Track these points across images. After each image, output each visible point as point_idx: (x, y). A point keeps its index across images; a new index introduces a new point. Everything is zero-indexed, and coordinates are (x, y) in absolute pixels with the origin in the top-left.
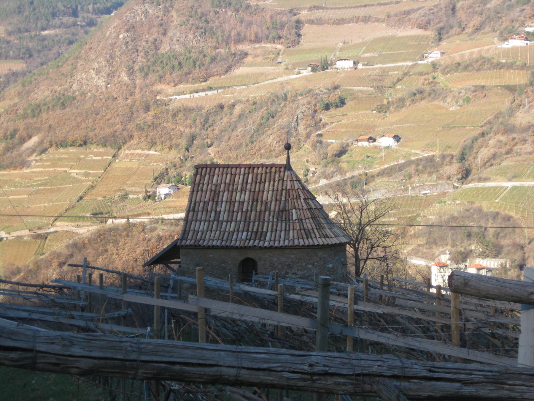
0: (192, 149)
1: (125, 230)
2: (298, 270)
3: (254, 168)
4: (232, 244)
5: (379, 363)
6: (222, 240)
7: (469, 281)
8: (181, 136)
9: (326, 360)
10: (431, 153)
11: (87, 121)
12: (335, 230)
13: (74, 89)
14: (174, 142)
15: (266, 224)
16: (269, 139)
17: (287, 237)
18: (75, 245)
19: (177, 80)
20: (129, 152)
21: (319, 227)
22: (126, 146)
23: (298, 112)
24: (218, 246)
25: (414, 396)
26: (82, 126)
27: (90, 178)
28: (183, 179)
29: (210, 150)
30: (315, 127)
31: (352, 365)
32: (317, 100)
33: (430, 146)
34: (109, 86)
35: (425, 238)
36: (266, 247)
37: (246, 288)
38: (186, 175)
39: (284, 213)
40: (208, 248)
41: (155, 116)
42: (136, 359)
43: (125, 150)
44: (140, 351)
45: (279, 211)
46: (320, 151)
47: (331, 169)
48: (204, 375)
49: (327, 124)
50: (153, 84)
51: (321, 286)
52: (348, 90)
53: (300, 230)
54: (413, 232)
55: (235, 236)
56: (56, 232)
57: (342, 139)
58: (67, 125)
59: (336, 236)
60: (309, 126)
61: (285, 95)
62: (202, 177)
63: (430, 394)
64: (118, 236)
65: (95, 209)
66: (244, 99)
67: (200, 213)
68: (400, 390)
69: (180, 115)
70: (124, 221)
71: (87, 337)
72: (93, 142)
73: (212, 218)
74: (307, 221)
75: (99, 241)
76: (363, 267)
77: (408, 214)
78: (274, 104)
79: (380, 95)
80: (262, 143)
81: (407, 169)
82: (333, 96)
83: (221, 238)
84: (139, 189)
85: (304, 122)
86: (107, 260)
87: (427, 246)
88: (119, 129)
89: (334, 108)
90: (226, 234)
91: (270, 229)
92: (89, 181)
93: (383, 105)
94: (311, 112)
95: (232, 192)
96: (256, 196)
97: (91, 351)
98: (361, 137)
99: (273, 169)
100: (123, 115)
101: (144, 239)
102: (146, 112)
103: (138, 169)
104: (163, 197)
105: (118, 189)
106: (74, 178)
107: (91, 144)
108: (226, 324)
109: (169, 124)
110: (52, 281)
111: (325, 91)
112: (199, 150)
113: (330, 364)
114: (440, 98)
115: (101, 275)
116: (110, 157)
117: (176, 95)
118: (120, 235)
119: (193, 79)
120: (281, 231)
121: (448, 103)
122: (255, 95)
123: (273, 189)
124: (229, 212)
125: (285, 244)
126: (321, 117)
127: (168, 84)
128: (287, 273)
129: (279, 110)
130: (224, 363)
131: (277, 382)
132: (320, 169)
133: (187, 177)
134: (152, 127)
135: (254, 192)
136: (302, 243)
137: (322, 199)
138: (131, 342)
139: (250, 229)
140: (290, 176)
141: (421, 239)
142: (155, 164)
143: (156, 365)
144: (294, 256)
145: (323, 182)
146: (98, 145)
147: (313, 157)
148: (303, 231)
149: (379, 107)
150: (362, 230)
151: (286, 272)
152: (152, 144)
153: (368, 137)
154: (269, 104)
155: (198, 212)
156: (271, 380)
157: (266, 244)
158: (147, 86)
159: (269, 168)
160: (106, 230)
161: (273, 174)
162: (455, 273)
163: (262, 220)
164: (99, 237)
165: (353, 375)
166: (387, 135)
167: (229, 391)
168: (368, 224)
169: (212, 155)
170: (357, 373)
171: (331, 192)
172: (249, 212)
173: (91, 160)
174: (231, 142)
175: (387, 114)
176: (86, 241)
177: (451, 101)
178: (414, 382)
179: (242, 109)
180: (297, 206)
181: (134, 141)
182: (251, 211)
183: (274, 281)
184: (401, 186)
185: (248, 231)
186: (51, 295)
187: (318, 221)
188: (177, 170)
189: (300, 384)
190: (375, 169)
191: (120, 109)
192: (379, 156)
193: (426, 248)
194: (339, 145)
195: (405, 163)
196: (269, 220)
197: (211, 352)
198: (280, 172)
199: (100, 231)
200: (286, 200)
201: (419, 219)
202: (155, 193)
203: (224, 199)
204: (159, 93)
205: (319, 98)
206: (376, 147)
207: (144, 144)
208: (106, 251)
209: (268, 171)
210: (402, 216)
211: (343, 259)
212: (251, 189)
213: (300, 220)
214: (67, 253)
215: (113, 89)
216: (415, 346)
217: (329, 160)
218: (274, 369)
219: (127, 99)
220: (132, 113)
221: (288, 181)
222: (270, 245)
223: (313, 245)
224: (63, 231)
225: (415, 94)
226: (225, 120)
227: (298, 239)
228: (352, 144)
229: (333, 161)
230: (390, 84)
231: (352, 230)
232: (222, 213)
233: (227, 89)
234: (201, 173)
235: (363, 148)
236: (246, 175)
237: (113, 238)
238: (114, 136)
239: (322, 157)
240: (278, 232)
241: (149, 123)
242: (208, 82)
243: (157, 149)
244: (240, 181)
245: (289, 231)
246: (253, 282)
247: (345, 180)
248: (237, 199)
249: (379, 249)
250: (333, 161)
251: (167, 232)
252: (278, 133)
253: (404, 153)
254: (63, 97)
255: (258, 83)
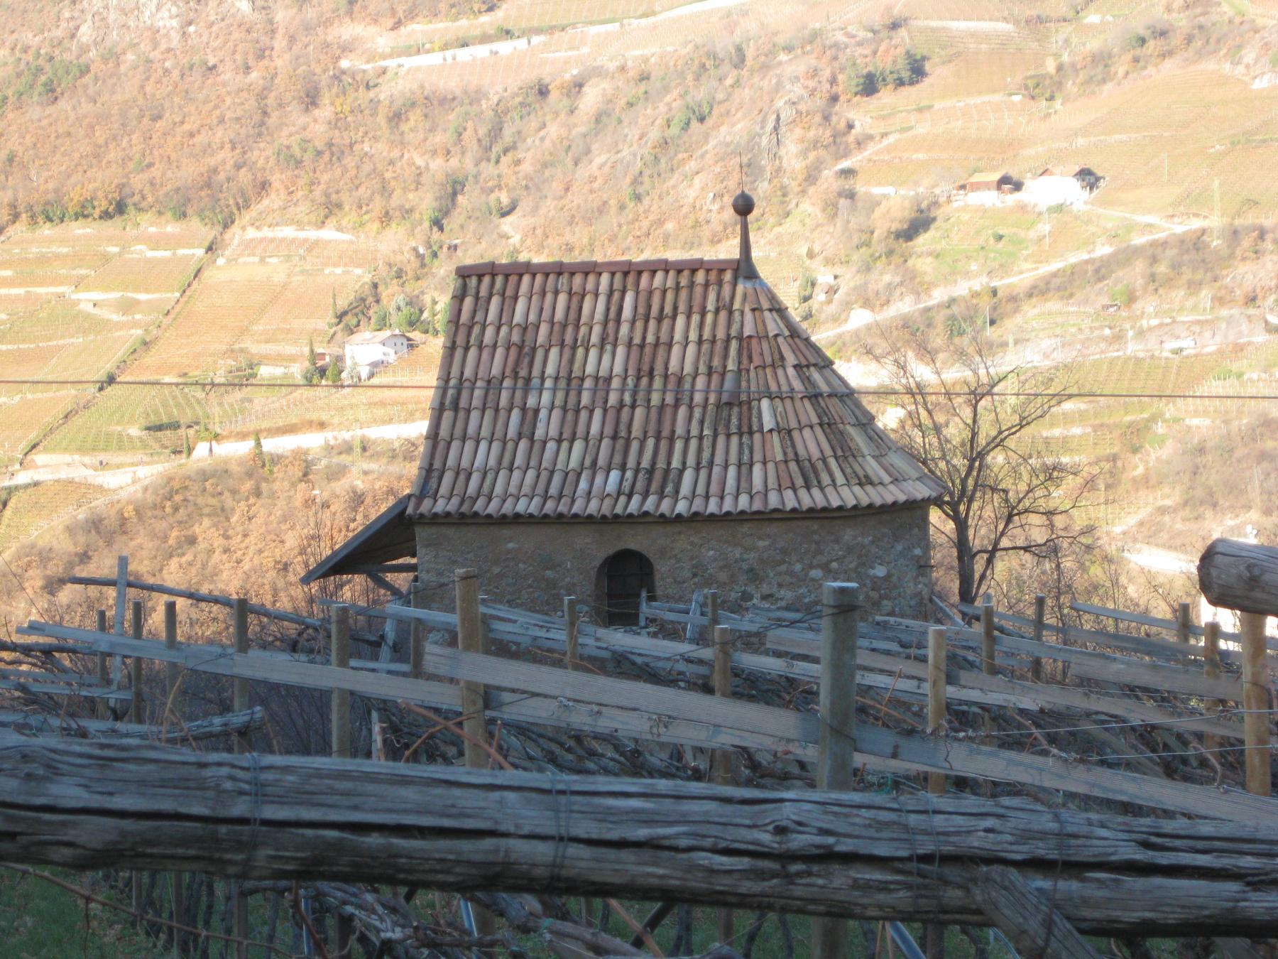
0: (450, 224)
1: (250, 475)
2: (780, 586)
3: (640, 273)
4: (576, 509)
5: (989, 822)
6: (546, 498)
7: (1263, 571)
8: (419, 183)
9: (826, 813)
10: (1196, 224)
11: (126, 139)
12: (895, 459)
13: (84, 39)
14: (396, 201)
15: (679, 445)
16: (690, 186)
17: (744, 485)
18: (95, 524)
19: (401, 10)
20: (259, 235)
21: (845, 452)
22: (247, 216)
23: (780, 103)
24: (531, 516)
25: (1099, 921)
26: (111, 156)
27: (138, 317)
28: (426, 315)
29: (507, 225)
30: (833, 148)
31: (906, 828)
32: (836, 64)
33: (1193, 201)
34: (192, 29)
35: (1178, 488)
36: (679, 516)
37: (619, 639)
38: (435, 303)
39: (736, 410)
40: (504, 521)
41: (337, 122)
42: (248, 815)
43: (244, 228)
44: (260, 792)
45: (718, 406)
46: (848, 222)
47: (885, 276)
48: (458, 862)
49: (871, 138)
50: (327, 23)
51: (830, 611)
52: (933, 30)
53: (786, 462)
54: (1140, 470)
55: (583, 485)
56: (36, 484)
57: (916, 184)
58: (64, 155)
59: (895, 481)
60: (815, 145)
61: (739, 49)
62: (481, 303)
63: (1148, 915)
64: (227, 494)
65: (156, 412)
66: (612, 66)
67: (475, 415)
68: (1056, 906)
69: (414, 117)
70: (246, 447)
71: (98, 752)
72: (144, 205)
73: (512, 432)
74: (807, 433)
75: (168, 510)
76: (983, 577)
77: (1127, 413)
78: (704, 79)
79: (1034, 45)
80: (670, 199)
81: (1120, 273)
82: (887, 51)
83: (540, 488)
84: (290, 350)
85: (798, 132)
86: (194, 571)
87: (1187, 512)
88: (224, 162)
89: (891, 87)
90: (557, 479)
91: (691, 461)
92: (135, 325)
93: (1044, 77)
94: (819, 102)
95: (574, 348)
96: (647, 359)
97: (111, 794)
98: (977, 178)
99: (700, 277)
100: (238, 119)
101: (309, 502)
102: (307, 110)
103: (285, 286)
104: (364, 372)
105: (224, 348)
106: (88, 316)
107: (140, 210)
108: (554, 747)
109: (379, 145)
110: (20, 631)
111: (862, 34)
112: (472, 226)
113: (840, 826)
114: (1223, 51)
115: (171, 607)
116: (200, 252)
117: (399, 56)
118: (234, 492)
119: (453, 6)
120: (726, 467)
121: (1248, 66)
122: (646, 52)
123: (701, 336)
124: (564, 409)
125: (740, 508)
126: (851, 115)
127: (375, 21)
128: (746, 597)
129: (720, 96)
130: (517, 826)
131: (678, 883)
132: (849, 279)
133: (438, 308)
134: (327, 157)
135: (642, 346)
136: (791, 502)
137: (857, 373)
138: (233, 766)
139: (631, 463)
140: (751, 298)
141: (1167, 490)
142: (339, 271)
143: (309, 832)
144: (767, 543)
145: (860, 318)
146: (160, 213)
147: (829, 239)
148: (793, 466)
149: (1031, 83)
150: (976, 457)
151: (744, 592)
152: (330, 209)
153: (996, 176)
154: (690, 77)
155: (468, 411)
156: (662, 877)
157: (681, 507)
158: (308, 29)
159: (686, 273)
160: (189, 478)
161: (698, 291)
162: (1220, 549)
163: (666, 433)
164: (170, 498)
165: (910, 859)
166: (1056, 170)
167: (551, 932)
168: (997, 442)
169: (516, 239)
170: (921, 852)
171: (881, 347)
172: (626, 410)
173: (139, 260)
174: (575, 200)
175: (1057, 104)
176: (129, 512)
177: (1256, 61)
178: (1098, 880)
179: (604, 95)
180: (773, 387)
181: (273, 201)
182: (633, 407)
183: (705, 621)
184: (1102, 327)
185: (623, 468)
186: (20, 674)
187: (842, 433)
188: (408, 288)
189: (747, 886)
190: (1022, 276)
191: (228, 101)
192: (1032, 234)
193: (1184, 520)
194: (907, 204)
195: (1113, 256)
196: (689, 431)
197: (476, 791)
198: (720, 283)
199: (170, 479)
200: (740, 370)
201: (1160, 429)
202: (339, 359)
203: (550, 370)
204: (346, 49)
205: (843, 58)
206: (1022, 208)
207: (303, 208)
208: (192, 541)
209: (684, 282)
210: (1106, 420)
211: (918, 552)
212: (631, 339)
213: (786, 433)
214: (72, 549)
215: (205, 38)
216: (1122, 792)
217: (879, 248)
218: (667, 843)
219: (247, 69)
220: (265, 113)
221: (747, 310)
222: (694, 509)
223: (824, 509)
224: (57, 481)
225: (1143, 41)
226: (553, 130)
227: (780, 490)
228: (949, 200)
229: (890, 253)
230: (1064, 10)
231: (948, 462)
232: (543, 414)
233: (557, 35)
234: (478, 292)
235: (983, 211)
236: (616, 296)
237: (211, 501)
238: (209, 185)
239: (856, 241)
240: (716, 470)
241: (319, 145)
242: (499, 14)
243: (344, 222)
244: (599, 315)
245: (751, 465)
246: (642, 623)
247: (928, 310)
248: (590, 369)
249: (1034, 519)
250: (890, 253)
251: (378, 479)
252: (718, 169)
253: (1110, 226)
254: (47, 68)
255: (654, 13)
